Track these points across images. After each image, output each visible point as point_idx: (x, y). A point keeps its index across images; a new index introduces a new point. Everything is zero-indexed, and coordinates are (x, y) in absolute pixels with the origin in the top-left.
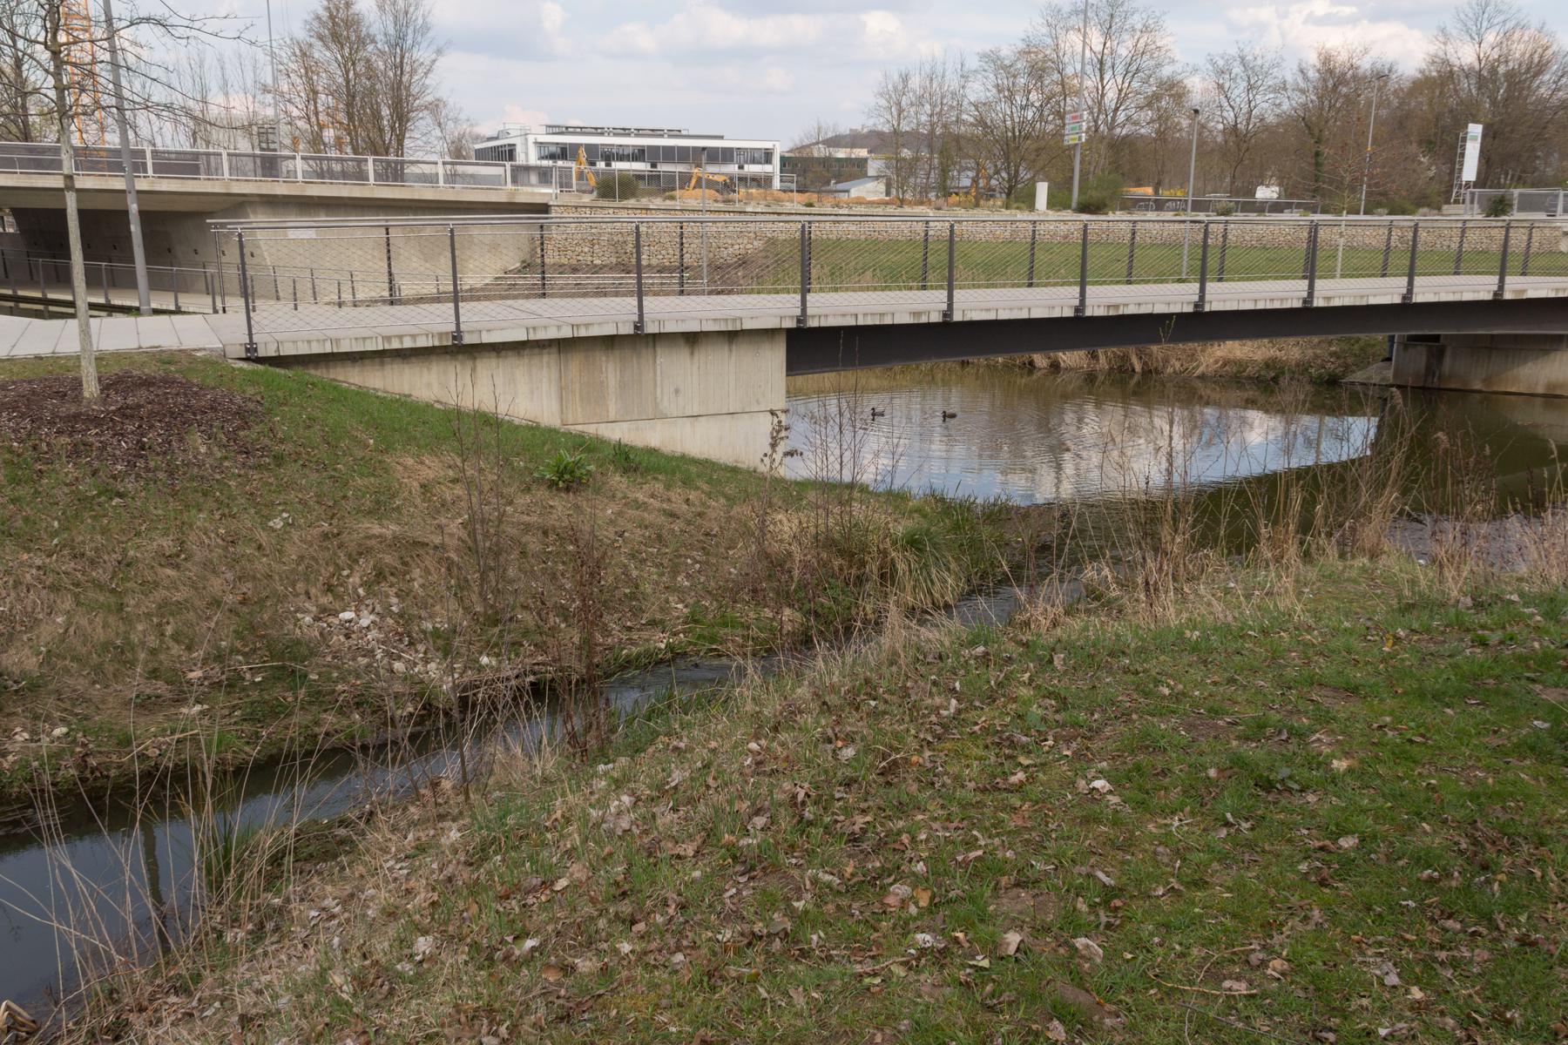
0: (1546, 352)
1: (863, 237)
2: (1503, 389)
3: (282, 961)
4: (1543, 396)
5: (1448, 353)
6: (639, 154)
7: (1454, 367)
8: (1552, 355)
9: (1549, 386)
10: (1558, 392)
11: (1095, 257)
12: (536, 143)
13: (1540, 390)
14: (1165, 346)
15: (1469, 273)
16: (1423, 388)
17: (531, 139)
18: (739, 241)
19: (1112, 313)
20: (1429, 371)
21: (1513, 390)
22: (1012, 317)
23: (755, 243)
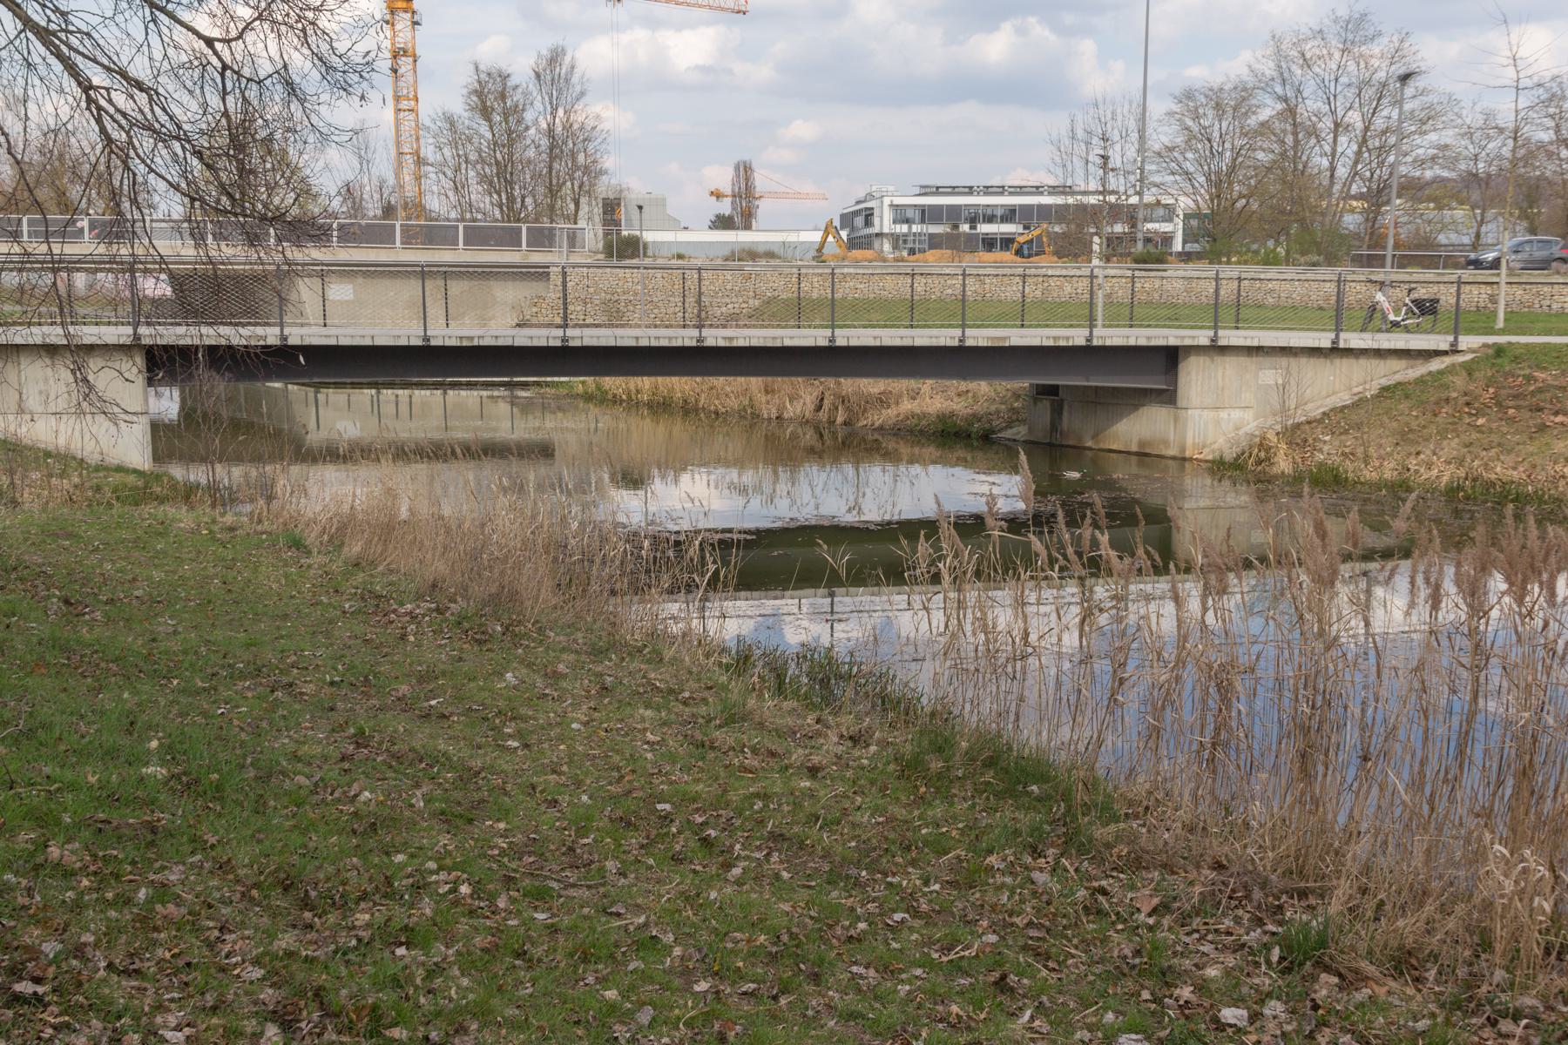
0: (1136, 407)
1: (872, 296)
2: (1107, 446)
3: (315, 889)
4: (1138, 454)
5: (1066, 407)
6: (1010, 215)
7: (1070, 420)
8: (1141, 411)
9: (1141, 444)
10: (1148, 451)
11: (827, 312)
12: (891, 205)
13: (1134, 449)
14: (197, 342)
15: (1141, 326)
16: (1050, 445)
17: (887, 201)
18: (734, 300)
19: (465, 343)
20: (1054, 427)
21: (1114, 447)
22: (355, 343)
23: (751, 302)
